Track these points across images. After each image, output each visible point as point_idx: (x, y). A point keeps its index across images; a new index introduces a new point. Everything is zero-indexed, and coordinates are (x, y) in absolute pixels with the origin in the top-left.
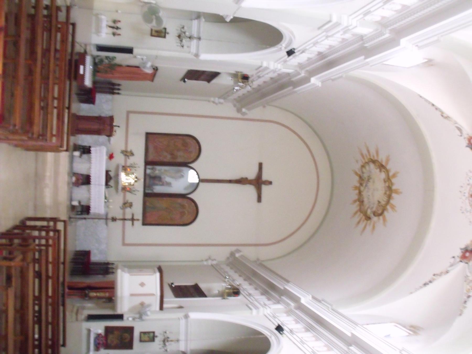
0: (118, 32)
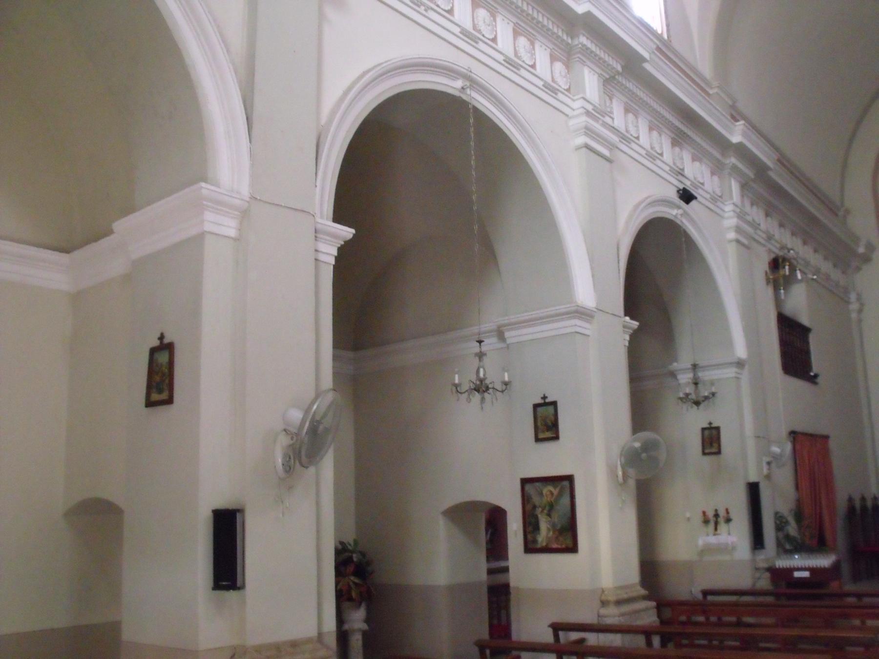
0: (722, 513)
